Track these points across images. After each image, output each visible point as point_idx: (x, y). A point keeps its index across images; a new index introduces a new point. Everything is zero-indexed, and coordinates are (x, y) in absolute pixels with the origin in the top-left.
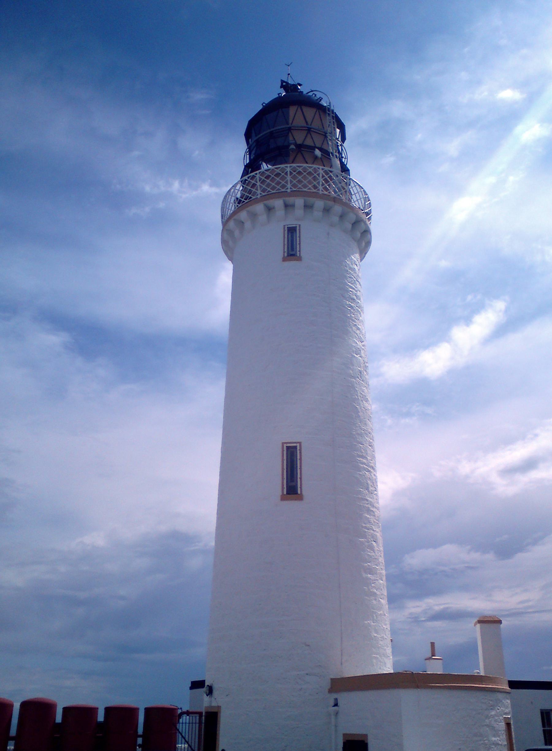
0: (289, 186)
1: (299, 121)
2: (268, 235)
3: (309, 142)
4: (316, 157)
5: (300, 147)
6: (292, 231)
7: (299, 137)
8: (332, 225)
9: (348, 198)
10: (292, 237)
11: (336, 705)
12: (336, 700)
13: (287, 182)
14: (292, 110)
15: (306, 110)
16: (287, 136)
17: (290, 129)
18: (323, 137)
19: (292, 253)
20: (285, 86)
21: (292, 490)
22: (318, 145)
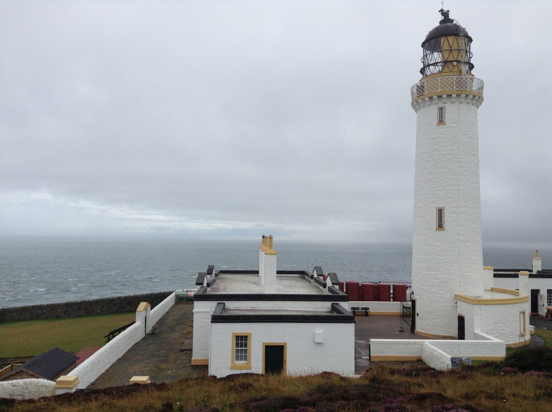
2: (432, 111)
6: (441, 109)
19: (441, 121)
21: (440, 226)
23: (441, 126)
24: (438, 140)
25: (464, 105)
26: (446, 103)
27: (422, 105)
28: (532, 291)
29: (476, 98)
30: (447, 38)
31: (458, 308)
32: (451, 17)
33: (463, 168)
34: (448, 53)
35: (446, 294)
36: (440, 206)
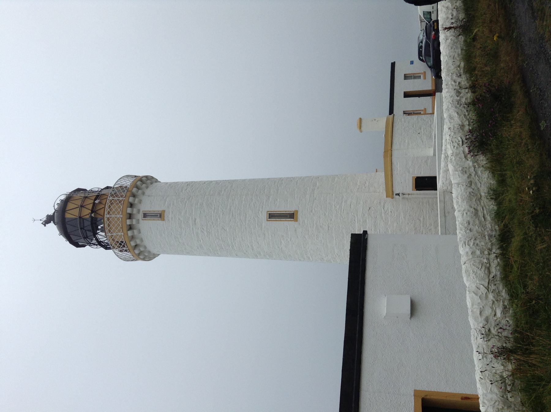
0: (118, 216)
1: (76, 212)
2: (148, 230)
3: (90, 207)
4: (100, 203)
5: (93, 211)
6: (145, 215)
7: (86, 212)
8: (143, 193)
9: (504, 215)
10: (149, 216)
11: (398, 194)
12: (396, 194)
13: (116, 217)
14: (68, 216)
15: (68, 208)
16: (83, 219)
17: (80, 217)
18: (87, 199)
19: (160, 216)
20: (46, 222)
21: (292, 216)
22: (93, 201)
23: (166, 216)
24: (182, 219)
25: (148, 192)
26: (139, 211)
27: (138, 242)
28: (405, 97)
29: (144, 182)
30: (83, 219)
31: (405, 192)
32: (51, 212)
33: (221, 191)
34: (84, 209)
35: (386, 209)
36: (265, 216)
